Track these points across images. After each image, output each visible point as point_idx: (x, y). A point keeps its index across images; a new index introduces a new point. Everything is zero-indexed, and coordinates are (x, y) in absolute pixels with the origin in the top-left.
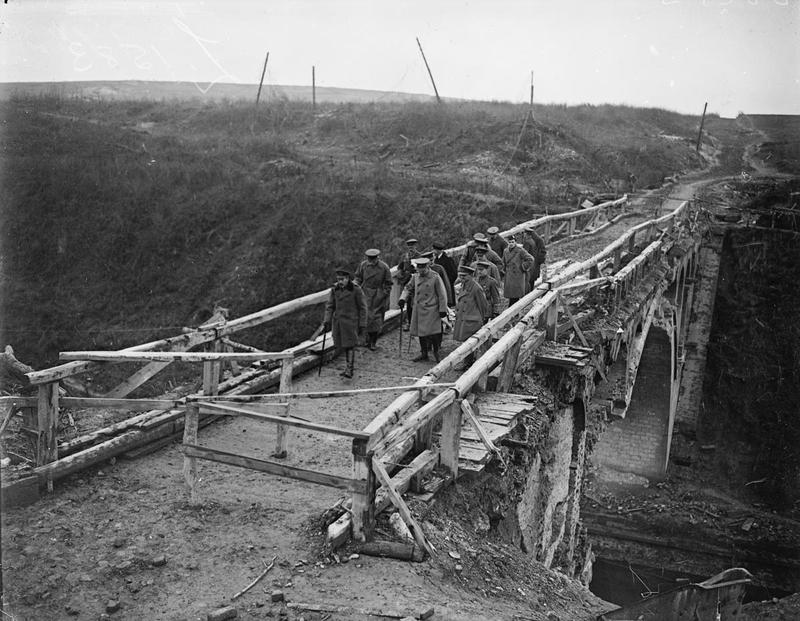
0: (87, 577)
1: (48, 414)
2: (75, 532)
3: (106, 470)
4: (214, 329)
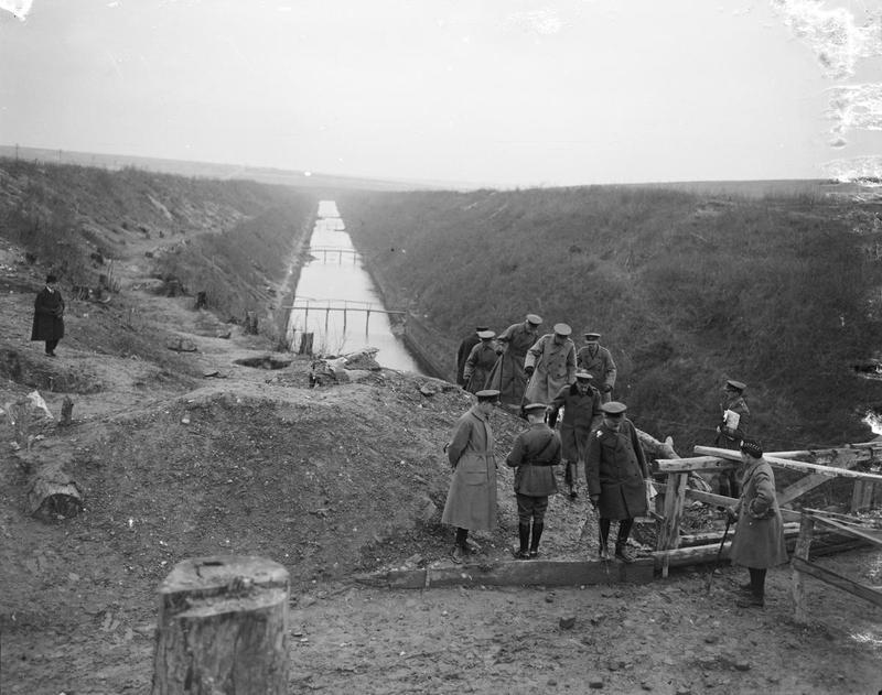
0: (669, 661)
1: (674, 502)
2: (675, 619)
3: (725, 570)
4: (870, 449)
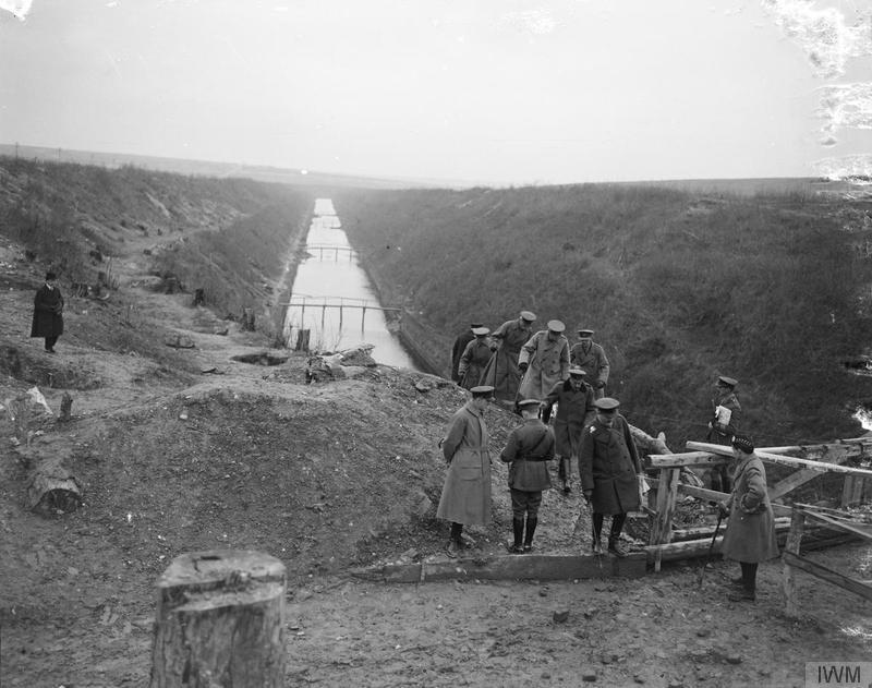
0: (662, 654)
1: (667, 497)
2: (667, 613)
3: (717, 564)
4: (860, 444)
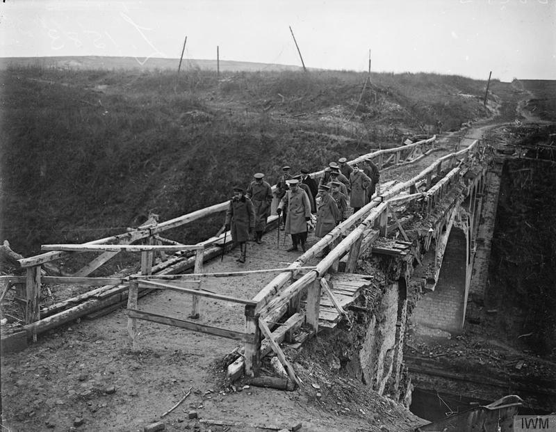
0: (60, 402)
1: (34, 288)
2: (52, 370)
3: (74, 327)
4: (149, 229)
